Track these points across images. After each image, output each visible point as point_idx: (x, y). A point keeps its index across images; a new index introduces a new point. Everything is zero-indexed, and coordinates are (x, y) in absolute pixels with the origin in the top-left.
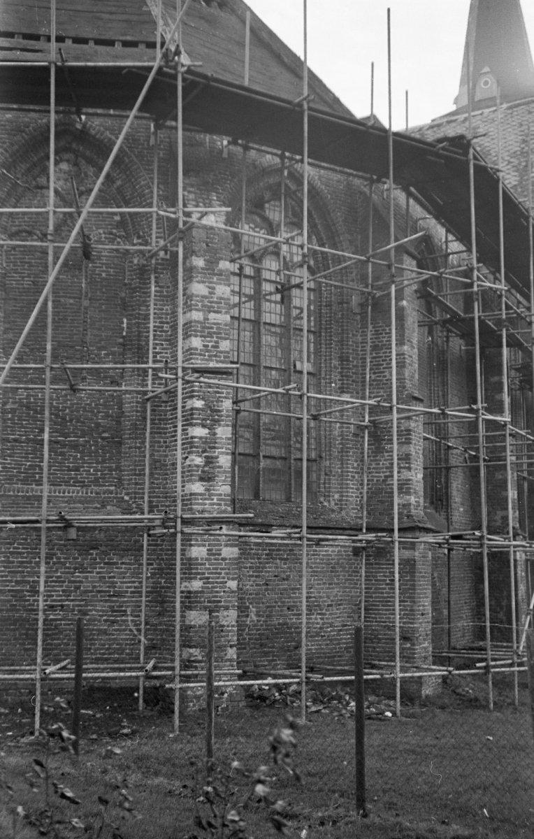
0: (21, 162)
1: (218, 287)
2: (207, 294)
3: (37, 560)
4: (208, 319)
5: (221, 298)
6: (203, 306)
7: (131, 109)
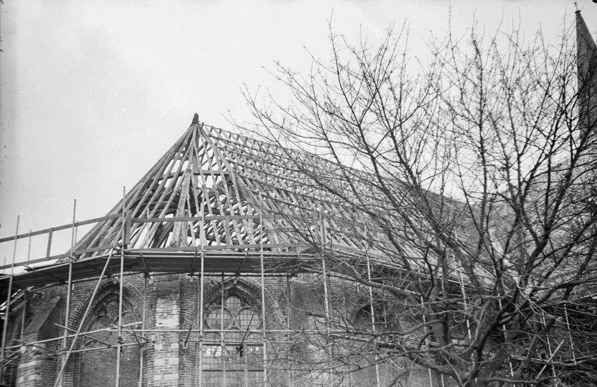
0: (57, 349)
1: (170, 359)
2: (164, 364)
3: (65, 383)
4: (164, 379)
5: (172, 365)
6: (161, 372)
7: (120, 272)
